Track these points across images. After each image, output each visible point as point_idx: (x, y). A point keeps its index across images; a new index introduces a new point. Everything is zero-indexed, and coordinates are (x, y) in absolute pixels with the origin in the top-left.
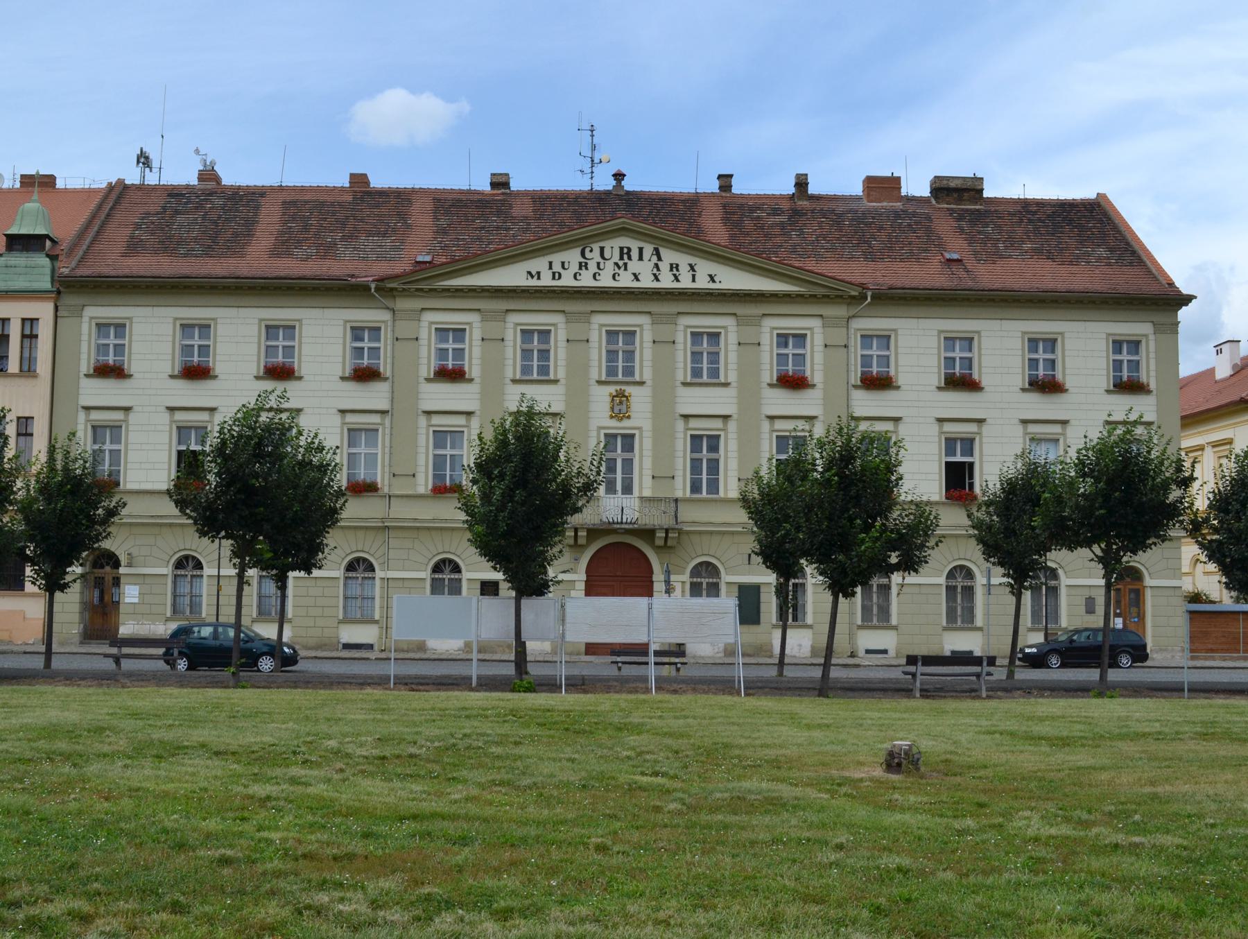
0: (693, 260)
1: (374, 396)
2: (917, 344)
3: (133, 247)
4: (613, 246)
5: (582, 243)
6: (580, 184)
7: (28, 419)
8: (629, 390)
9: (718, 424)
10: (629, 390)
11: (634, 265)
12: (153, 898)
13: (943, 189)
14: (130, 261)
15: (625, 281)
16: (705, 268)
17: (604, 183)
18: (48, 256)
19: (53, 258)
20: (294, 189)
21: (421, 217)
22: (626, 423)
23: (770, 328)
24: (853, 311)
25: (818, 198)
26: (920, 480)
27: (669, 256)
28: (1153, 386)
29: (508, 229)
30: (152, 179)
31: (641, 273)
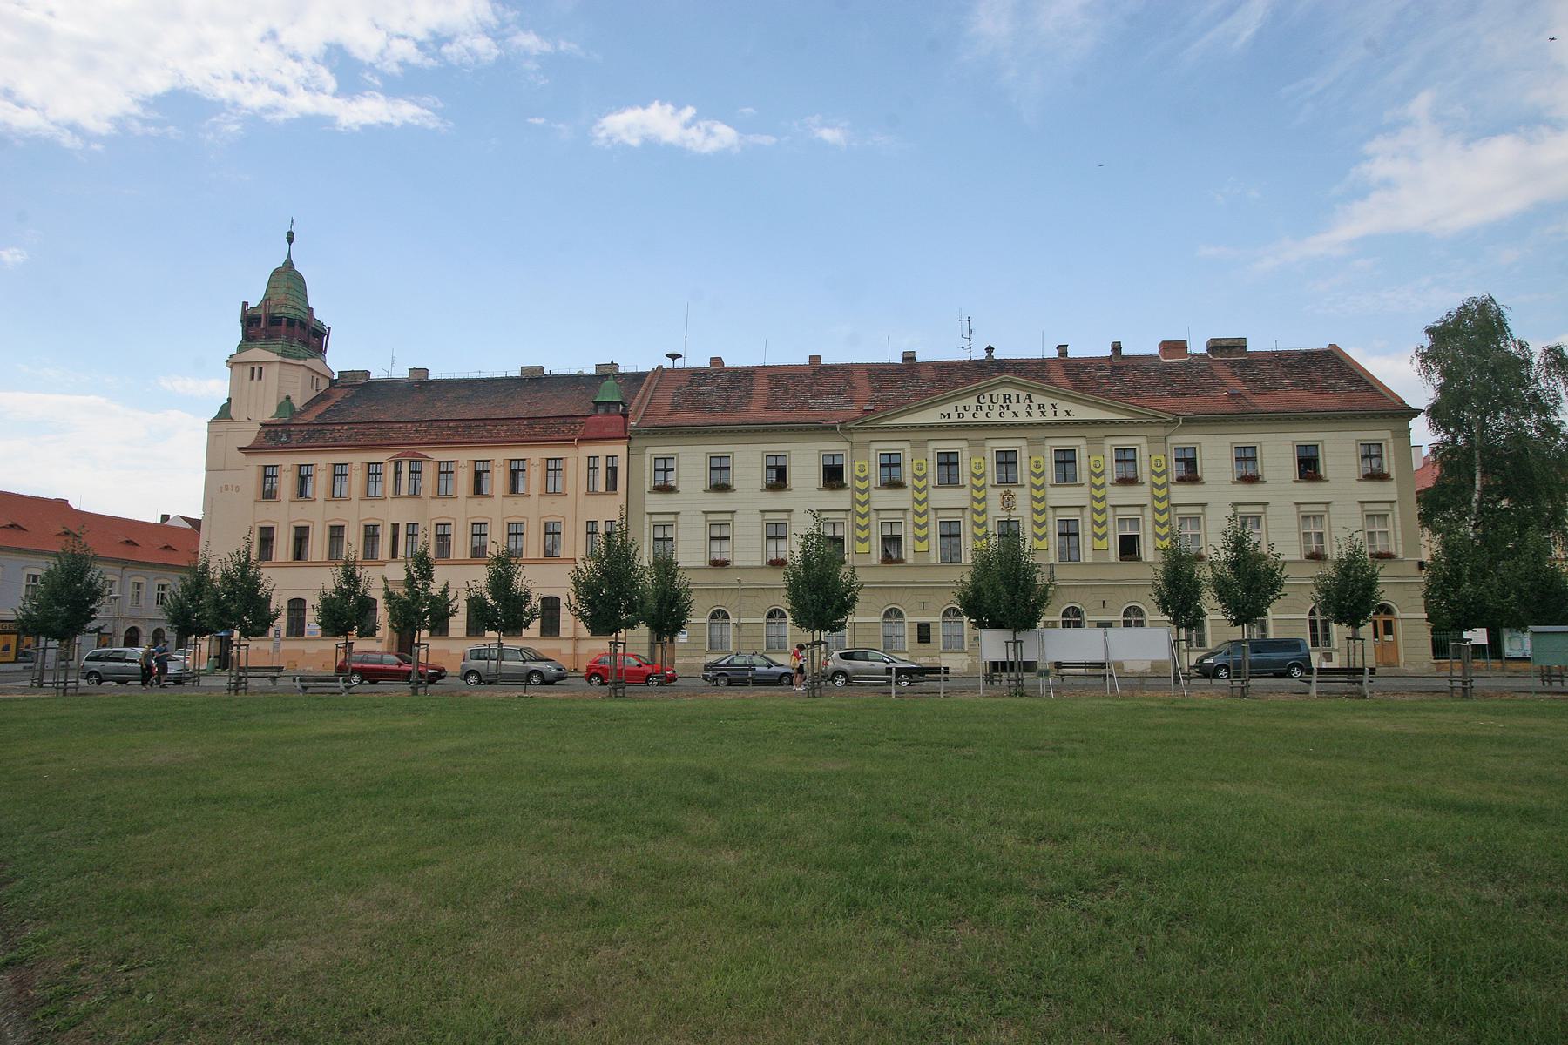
0: (1054, 401)
1: (841, 499)
3: (675, 408)
4: (999, 394)
6: (964, 356)
9: (1077, 511)
11: (1014, 406)
12: (1082, 834)
13: (1216, 347)
14: (674, 417)
15: (1008, 417)
16: (1062, 406)
17: (979, 354)
20: (773, 367)
23: (1113, 443)
24: (1170, 430)
25: (1128, 357)
27: (1038, 399)
28: (1393, 475)
30: (679, 364)
31: (1020, 411)
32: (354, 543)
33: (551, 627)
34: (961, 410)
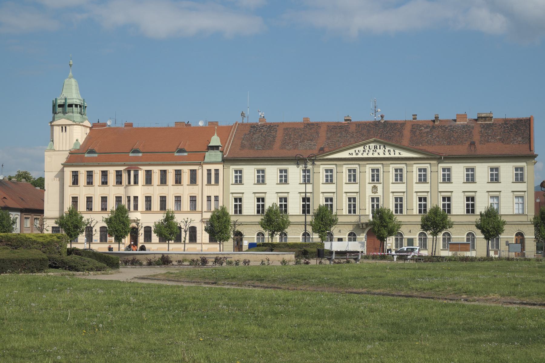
2: (458, 170)
4: (372, 145)
5: (364, 145)
7: (217, 196)
8: (377, 185)
10: (377, 185)
11: (378, 151)
15: (376, 155)
16: (397, 151)
18: (221, 151)
19: (222, 152)
21: (323, 133)
22: (376, 194)
26: (458, 207)
29: (347, 137)
30: (245, 121)
32: (171, 205)
33: (193, 238)
34: (357, 152)
